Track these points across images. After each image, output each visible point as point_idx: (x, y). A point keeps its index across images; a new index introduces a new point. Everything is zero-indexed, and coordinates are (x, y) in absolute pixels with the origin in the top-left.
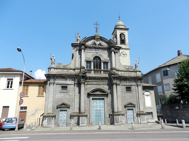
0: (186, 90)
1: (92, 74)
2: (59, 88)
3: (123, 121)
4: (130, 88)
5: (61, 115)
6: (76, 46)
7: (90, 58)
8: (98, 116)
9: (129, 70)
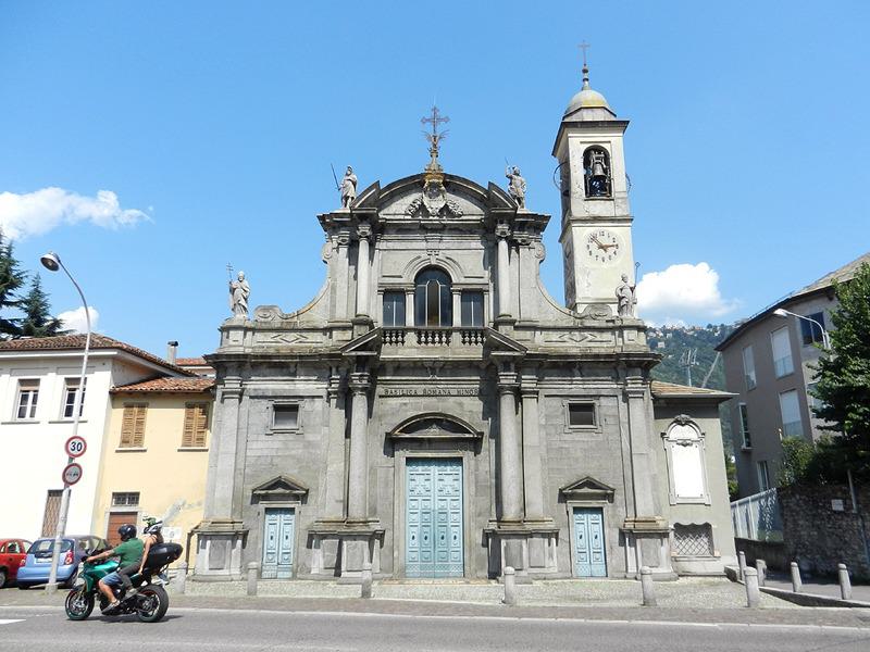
0: (860, 414)
1: (410, 349)
2: (263, 413)
3: (548, 562)
4: (590, 407)
5: (269, 530)
6: (337, 224)
7: (400, 277)
8: (433, 535)
9: (588, 323)
